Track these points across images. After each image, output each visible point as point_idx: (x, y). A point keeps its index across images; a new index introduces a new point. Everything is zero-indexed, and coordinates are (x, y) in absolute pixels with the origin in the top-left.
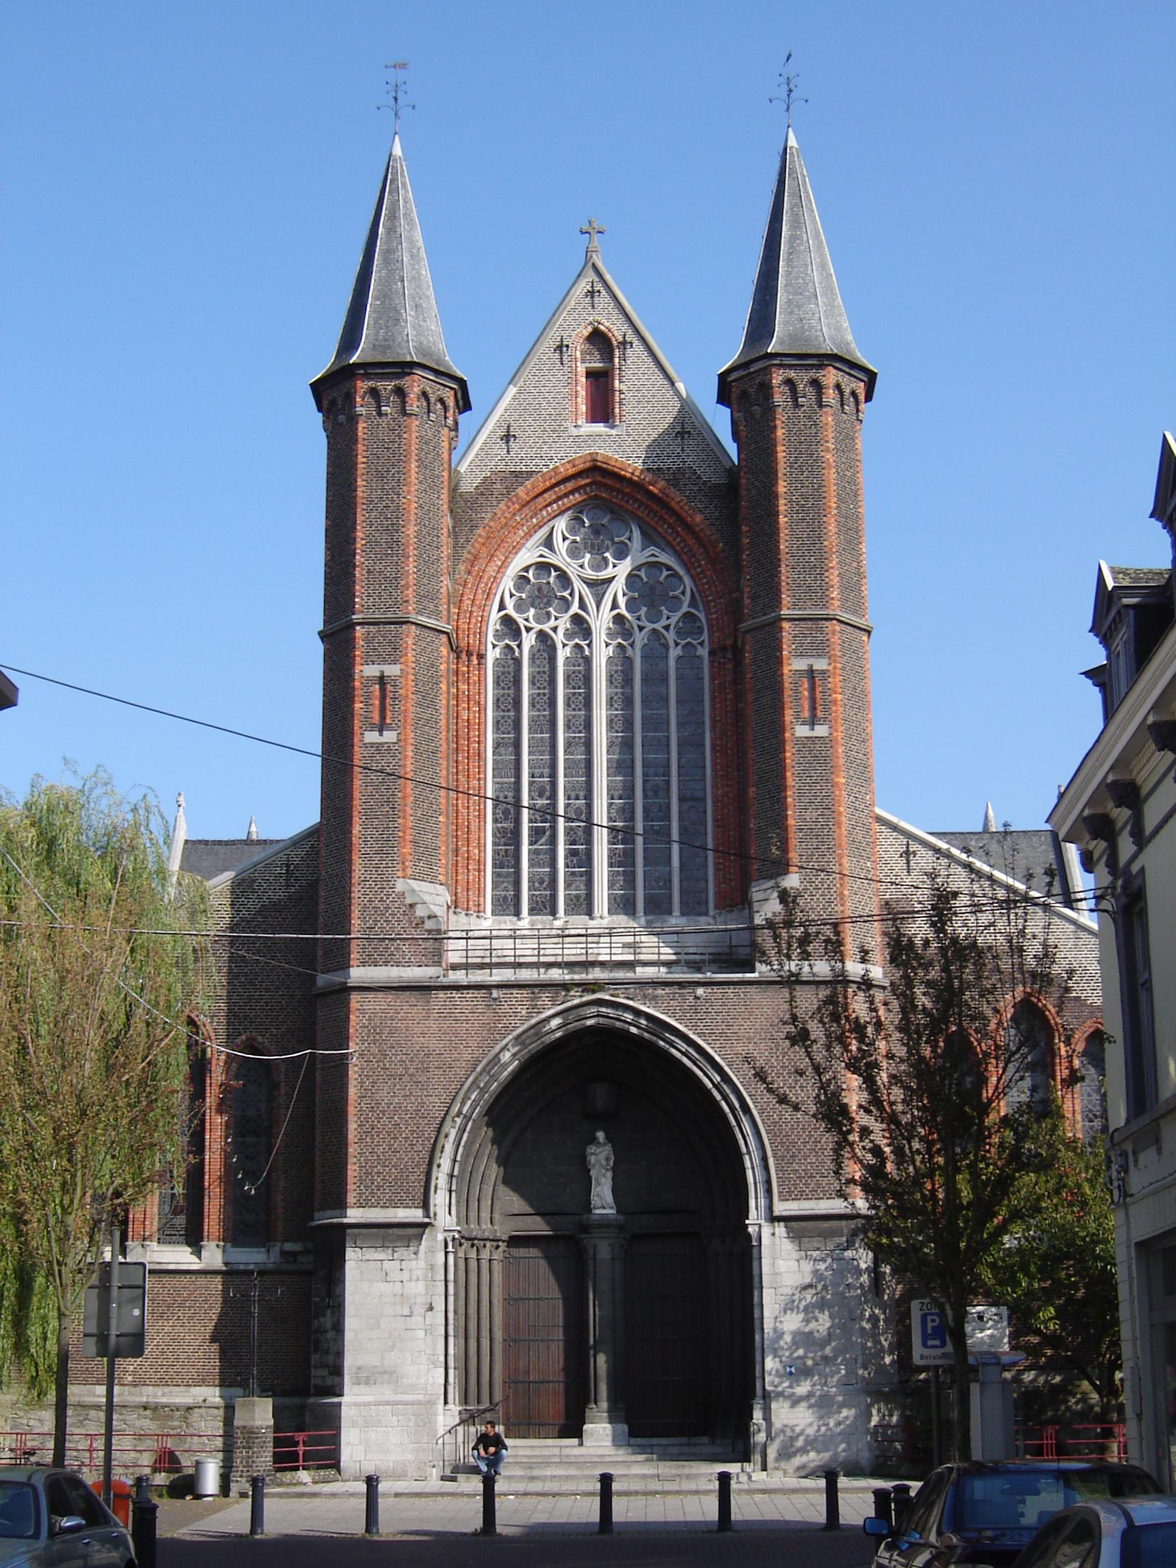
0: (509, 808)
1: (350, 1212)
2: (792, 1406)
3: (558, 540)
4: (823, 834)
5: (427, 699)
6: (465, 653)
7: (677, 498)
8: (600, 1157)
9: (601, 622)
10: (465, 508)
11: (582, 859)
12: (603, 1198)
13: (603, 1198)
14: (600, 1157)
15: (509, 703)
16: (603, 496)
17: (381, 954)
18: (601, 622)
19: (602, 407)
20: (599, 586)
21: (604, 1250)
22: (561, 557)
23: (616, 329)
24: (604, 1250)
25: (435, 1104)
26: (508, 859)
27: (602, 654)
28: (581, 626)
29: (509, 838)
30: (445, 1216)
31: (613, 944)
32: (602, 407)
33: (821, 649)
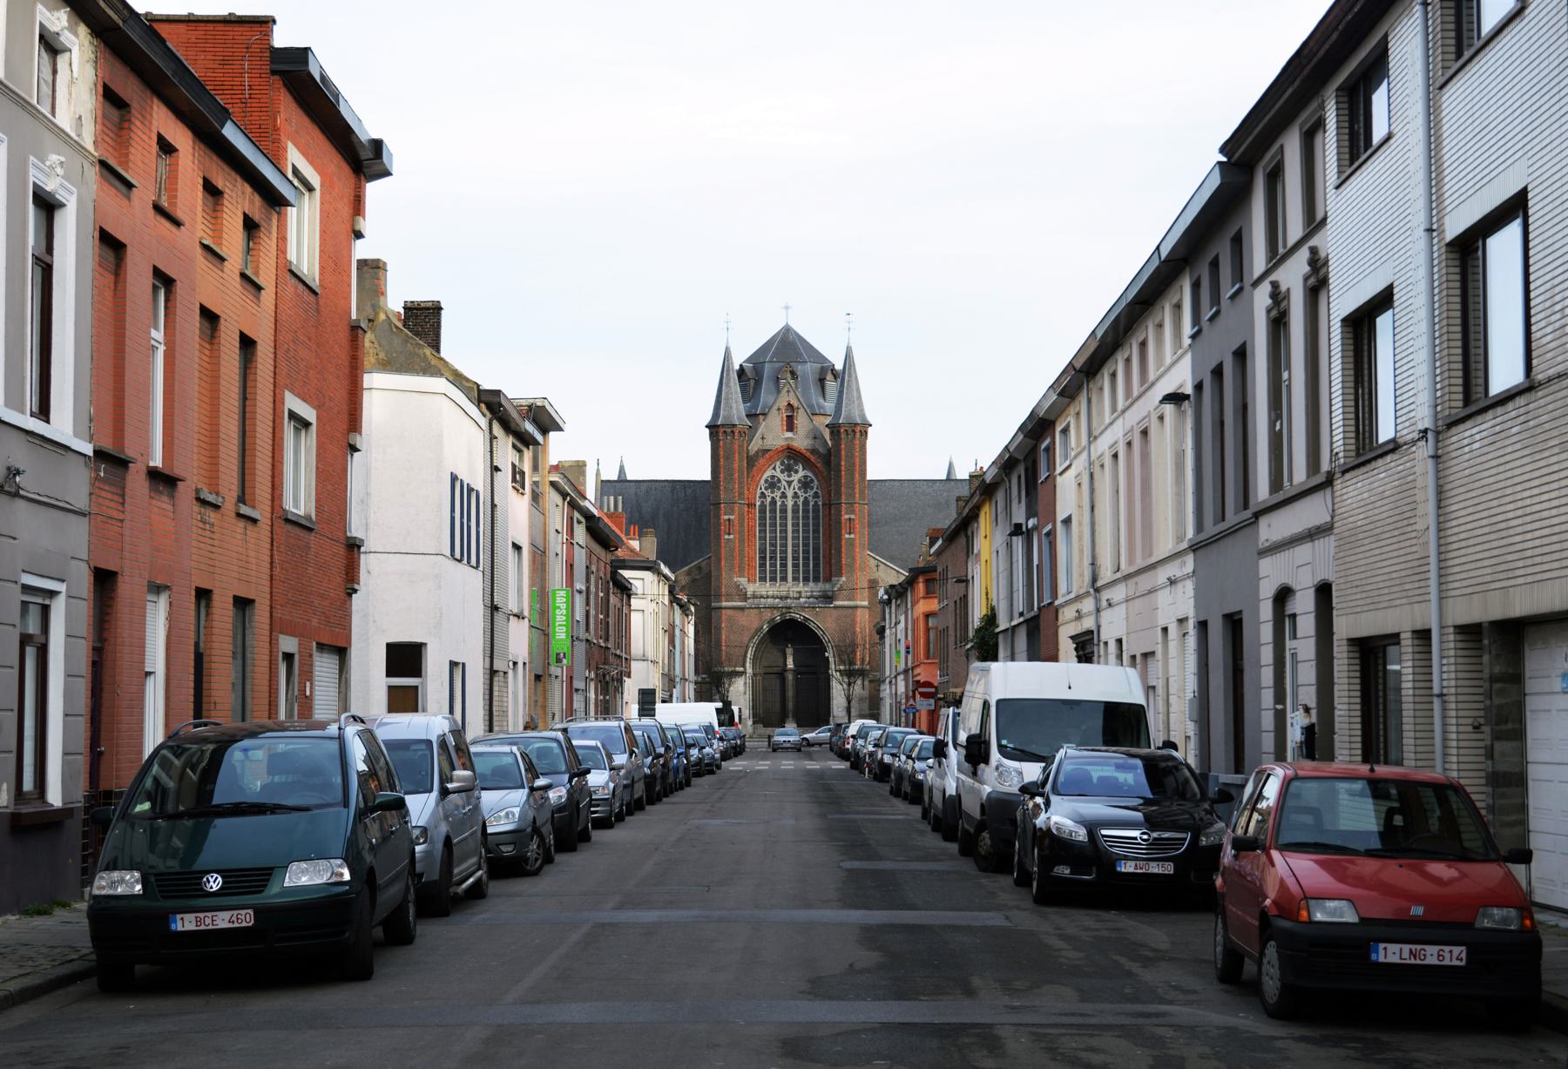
0: (763, 551)
1: (31, 631)
2: (545, 421)
3: (775, 471)
4: (851, 566)
5: (742, 525)
6: (751, 505)
7: (812, 458)
8: (789, 651)
9: (790, 494)
10: (751, 461)
11: (784, 565)
12: (790, 664)
13: (790, 664)
14: (789, 651)
15: (763, 518)
16: (792, 456)
17: (730, 598)
18: (790, 494)
19: (790, 427)
20: (789, 483)
21: (790, 677)
22: (778, 473)
23: (795, 403)
24: (790, 677)
25: (746, 639)
26: (763, 565)
27: (790, 503)
28: (784, 496)
29: (763, 558)
30: (749, 670)
31: (790, 592)
32: (790, 427)
33: (853, 512)
